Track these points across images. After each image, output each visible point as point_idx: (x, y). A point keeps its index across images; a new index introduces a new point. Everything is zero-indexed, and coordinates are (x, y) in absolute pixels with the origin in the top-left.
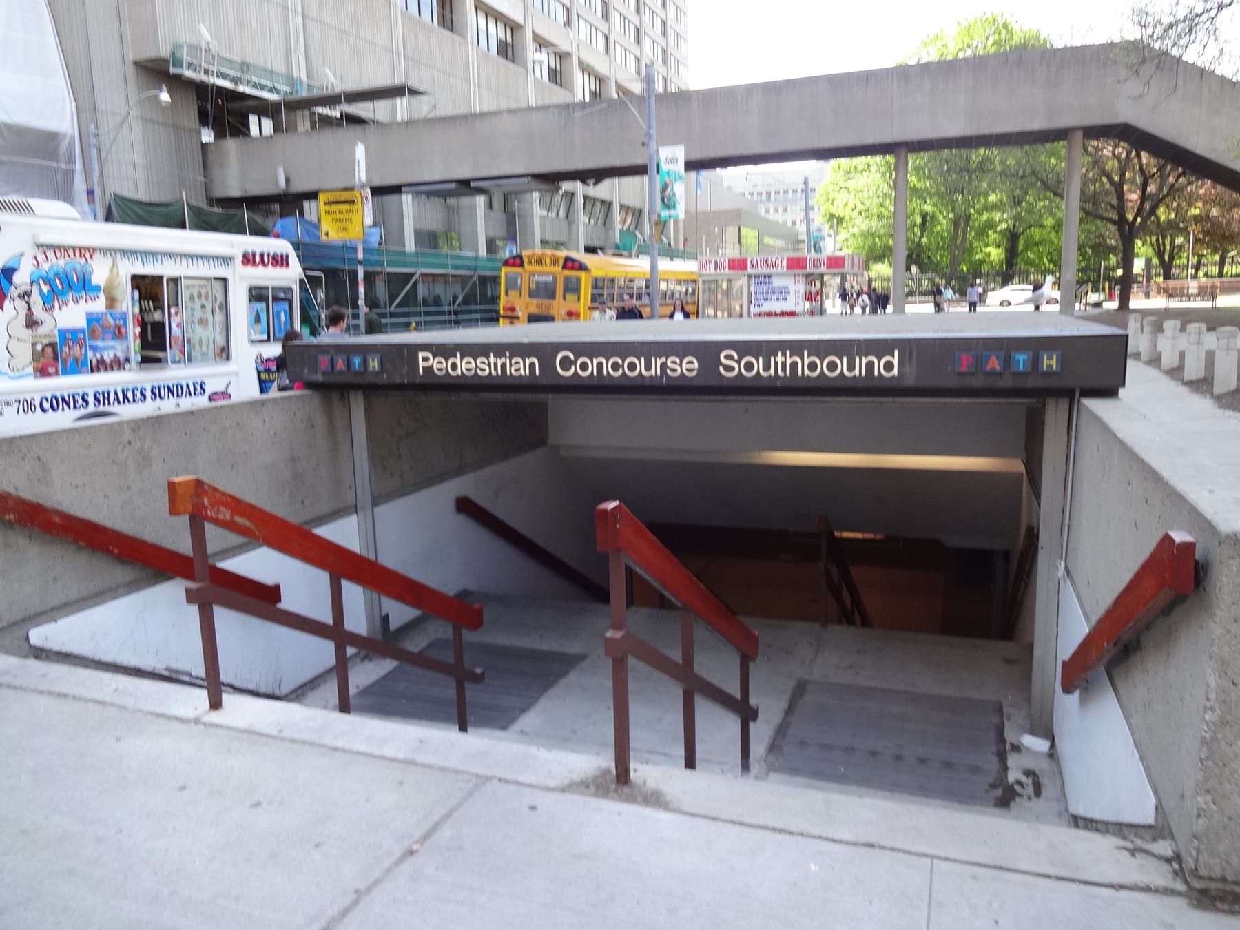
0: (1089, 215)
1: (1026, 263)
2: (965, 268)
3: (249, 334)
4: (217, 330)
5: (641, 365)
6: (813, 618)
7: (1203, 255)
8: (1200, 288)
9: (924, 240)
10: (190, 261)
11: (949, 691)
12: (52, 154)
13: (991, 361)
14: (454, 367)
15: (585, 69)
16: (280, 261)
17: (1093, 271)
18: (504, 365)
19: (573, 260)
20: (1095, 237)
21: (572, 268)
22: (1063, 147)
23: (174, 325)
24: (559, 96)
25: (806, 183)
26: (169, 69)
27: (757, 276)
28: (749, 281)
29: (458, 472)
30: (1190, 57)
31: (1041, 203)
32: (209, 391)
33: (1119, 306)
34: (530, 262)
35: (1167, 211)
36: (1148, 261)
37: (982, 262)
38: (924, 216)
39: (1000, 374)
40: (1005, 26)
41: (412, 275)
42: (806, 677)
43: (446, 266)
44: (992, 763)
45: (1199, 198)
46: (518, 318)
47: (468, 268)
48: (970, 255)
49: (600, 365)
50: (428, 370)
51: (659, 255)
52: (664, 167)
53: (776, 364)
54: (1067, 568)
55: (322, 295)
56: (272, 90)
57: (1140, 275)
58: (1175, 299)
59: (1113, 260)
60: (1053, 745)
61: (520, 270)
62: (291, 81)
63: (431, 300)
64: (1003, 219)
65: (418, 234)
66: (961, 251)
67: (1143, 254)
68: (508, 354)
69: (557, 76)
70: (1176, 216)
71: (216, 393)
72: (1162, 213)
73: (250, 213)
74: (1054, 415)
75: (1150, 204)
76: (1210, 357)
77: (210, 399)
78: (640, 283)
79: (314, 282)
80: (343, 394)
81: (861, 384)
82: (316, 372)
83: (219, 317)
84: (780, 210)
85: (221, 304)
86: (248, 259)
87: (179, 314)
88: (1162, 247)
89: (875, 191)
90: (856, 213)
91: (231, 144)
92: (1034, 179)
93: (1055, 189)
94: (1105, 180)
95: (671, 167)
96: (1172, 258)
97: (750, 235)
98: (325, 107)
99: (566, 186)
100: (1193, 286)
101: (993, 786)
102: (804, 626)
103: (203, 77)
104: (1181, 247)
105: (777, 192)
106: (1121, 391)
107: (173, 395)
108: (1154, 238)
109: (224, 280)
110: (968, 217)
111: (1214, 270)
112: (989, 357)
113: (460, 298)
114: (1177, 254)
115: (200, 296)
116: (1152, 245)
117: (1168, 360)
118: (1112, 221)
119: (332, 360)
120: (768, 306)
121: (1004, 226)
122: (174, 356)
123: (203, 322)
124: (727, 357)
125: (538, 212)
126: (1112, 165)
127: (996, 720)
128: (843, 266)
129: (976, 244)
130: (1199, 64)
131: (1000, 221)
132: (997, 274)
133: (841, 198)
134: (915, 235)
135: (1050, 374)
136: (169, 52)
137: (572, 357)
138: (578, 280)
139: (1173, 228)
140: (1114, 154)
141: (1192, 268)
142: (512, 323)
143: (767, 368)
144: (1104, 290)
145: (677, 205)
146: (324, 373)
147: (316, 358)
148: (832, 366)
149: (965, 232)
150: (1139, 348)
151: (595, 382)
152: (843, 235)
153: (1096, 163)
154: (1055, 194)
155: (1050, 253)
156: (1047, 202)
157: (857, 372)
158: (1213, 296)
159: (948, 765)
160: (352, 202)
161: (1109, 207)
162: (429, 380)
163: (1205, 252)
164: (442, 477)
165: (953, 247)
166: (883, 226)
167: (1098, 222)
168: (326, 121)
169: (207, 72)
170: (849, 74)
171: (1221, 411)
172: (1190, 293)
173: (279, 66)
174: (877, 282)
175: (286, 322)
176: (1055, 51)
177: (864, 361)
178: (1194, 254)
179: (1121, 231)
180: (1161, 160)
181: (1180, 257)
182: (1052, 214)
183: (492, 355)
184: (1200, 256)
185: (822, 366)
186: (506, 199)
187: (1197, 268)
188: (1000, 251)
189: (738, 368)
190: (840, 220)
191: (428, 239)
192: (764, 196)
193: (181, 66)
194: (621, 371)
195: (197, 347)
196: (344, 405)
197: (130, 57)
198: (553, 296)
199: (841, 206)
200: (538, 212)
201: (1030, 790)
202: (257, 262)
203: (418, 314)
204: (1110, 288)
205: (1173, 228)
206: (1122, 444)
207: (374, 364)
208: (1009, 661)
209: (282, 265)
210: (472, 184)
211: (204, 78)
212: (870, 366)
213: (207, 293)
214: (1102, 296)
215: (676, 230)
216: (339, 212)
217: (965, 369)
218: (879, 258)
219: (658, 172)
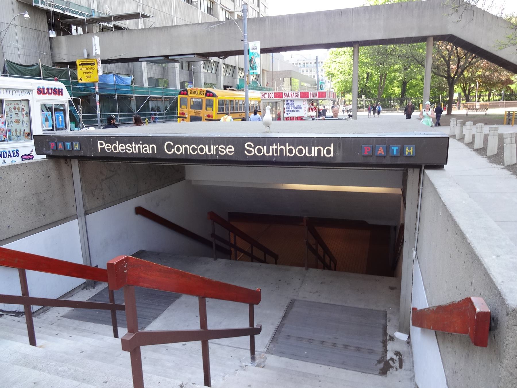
0: (436, 74)
1: (410, 94)
2: (384, 96)
3: (43, 127)
5: (206, 149)
8: (481, 106)
9: (368, 84)
11: (362, 306)
14: (115, 148)
18: (139, 147)
19: (210, 92)
20: (438, 84)
21: (209, 96)
24: (212, 19)
25: (317, 59)
27: (287, 101)
28: (283, 102)
29: (136, 195)
33: (447, 114)
35: (468, 73)
36: (460, 94)
37: (392, 94)
38: (368, 74)
39: (385, 157)
41: (147, 97)
42: (295, 298)
43: (161, 94)
44: (379, 348)
46: (186, 118)
48: (386, 91)
49: (186, 148)
50: (103, 149)
52: (251, 51)
53: (273, 149)
56: (81, 14)
57: (456, 100)
58: (470, 110)
59: (445, 93)
60: (409, 337)
61: (186, 96)
62: (90, 10)
64: (400, 76)
65: (149, 79)
66: (383, 89)
68: (141, 142)
71: (25, 155)
72: (466, 74)
75: (461, 69)
76: (486, 137)
77: (23, 159)
79: (76, 102)
80: (66, 160)
81: (314, 161)
82: (49, 150)
86: (40, 91)
89: (347, 63)
92: (412, 59)
93: (421, 63)
94: (442, 59)
96: (469, 93)
97: (295, 81)
98: (106, 23)
99: (213, 59)
100: (478, 105)
101: (379, 362)
102: (297, 269)
104: (473, 88)
105: (307, 63)
106: (445, 166)
108: (462, 84)
109: (27, 101)
110: (386, 74)
111: (486, 98)
114: (471, 91)
115: (15, 109)
116: (461, 87)
117: (468, 139)
119: (56, 143)
120: (292, 114)
121: (401, 78)
123: (17, 121)
124: (248, 146)
125: (203, 70)
126: (445, 53)
127: (383, 322)
128: (325, 97)
129: (389, 86)
131: (399, 76)
132: (397, 99)
133: (333, 65)
134: (364, 82)
135: (409, 157)
137: (172, 144)
138: (212, 101)
139: (471, 80)
141: (477, 97)
142: (183, 120)
143: (268, 152)
146: (53, 150)
147: (49, 143)
148: (300, 151)
149: (384, 81)
150: (455, 133)
151: (184, 158)
152: (334, 81)
153: (439, 51)
155: (419, 90)
157: (313, 155)
158: (486, 109)
159: (358, 349)
160: (92, 64)
161: (444, 71)
164: (127, 198)
165: (380, 87)
166: (350, 78)
168: (105, 29)
169: (50, 5)
170: (334, 11)
171: (491, 164)
172: (476, 108)
174: (348, 102)
175: (62, 121)
177: (316, 148)
178: (478, 91)
179: (448, 81)
180: (466, 51)
182: (420, 74)
184: (481, 92)
185: (295, 151)
187: (479, 97)
188: (399, 89)
189: (254, 151)
190: (332, 75)
191: (154, 82)
192: (302, 65)
194: (196, 152)
195: (14, 133)
196: (68, 166)
198: (201, 109)
199: (333, 69)
200: (203, 70)
201: (397, 364)
202: (45, 92)
203: (149, 115)
205: (471, 80)
206: (444, 205)
207: (76, 146)
209: (59, 94)
210: (170, 58)
211: (49, 8)
212: (319, 151)
215: (263, 79)
216: (87, 69)
218: (349, 92)
219: (248, 54)
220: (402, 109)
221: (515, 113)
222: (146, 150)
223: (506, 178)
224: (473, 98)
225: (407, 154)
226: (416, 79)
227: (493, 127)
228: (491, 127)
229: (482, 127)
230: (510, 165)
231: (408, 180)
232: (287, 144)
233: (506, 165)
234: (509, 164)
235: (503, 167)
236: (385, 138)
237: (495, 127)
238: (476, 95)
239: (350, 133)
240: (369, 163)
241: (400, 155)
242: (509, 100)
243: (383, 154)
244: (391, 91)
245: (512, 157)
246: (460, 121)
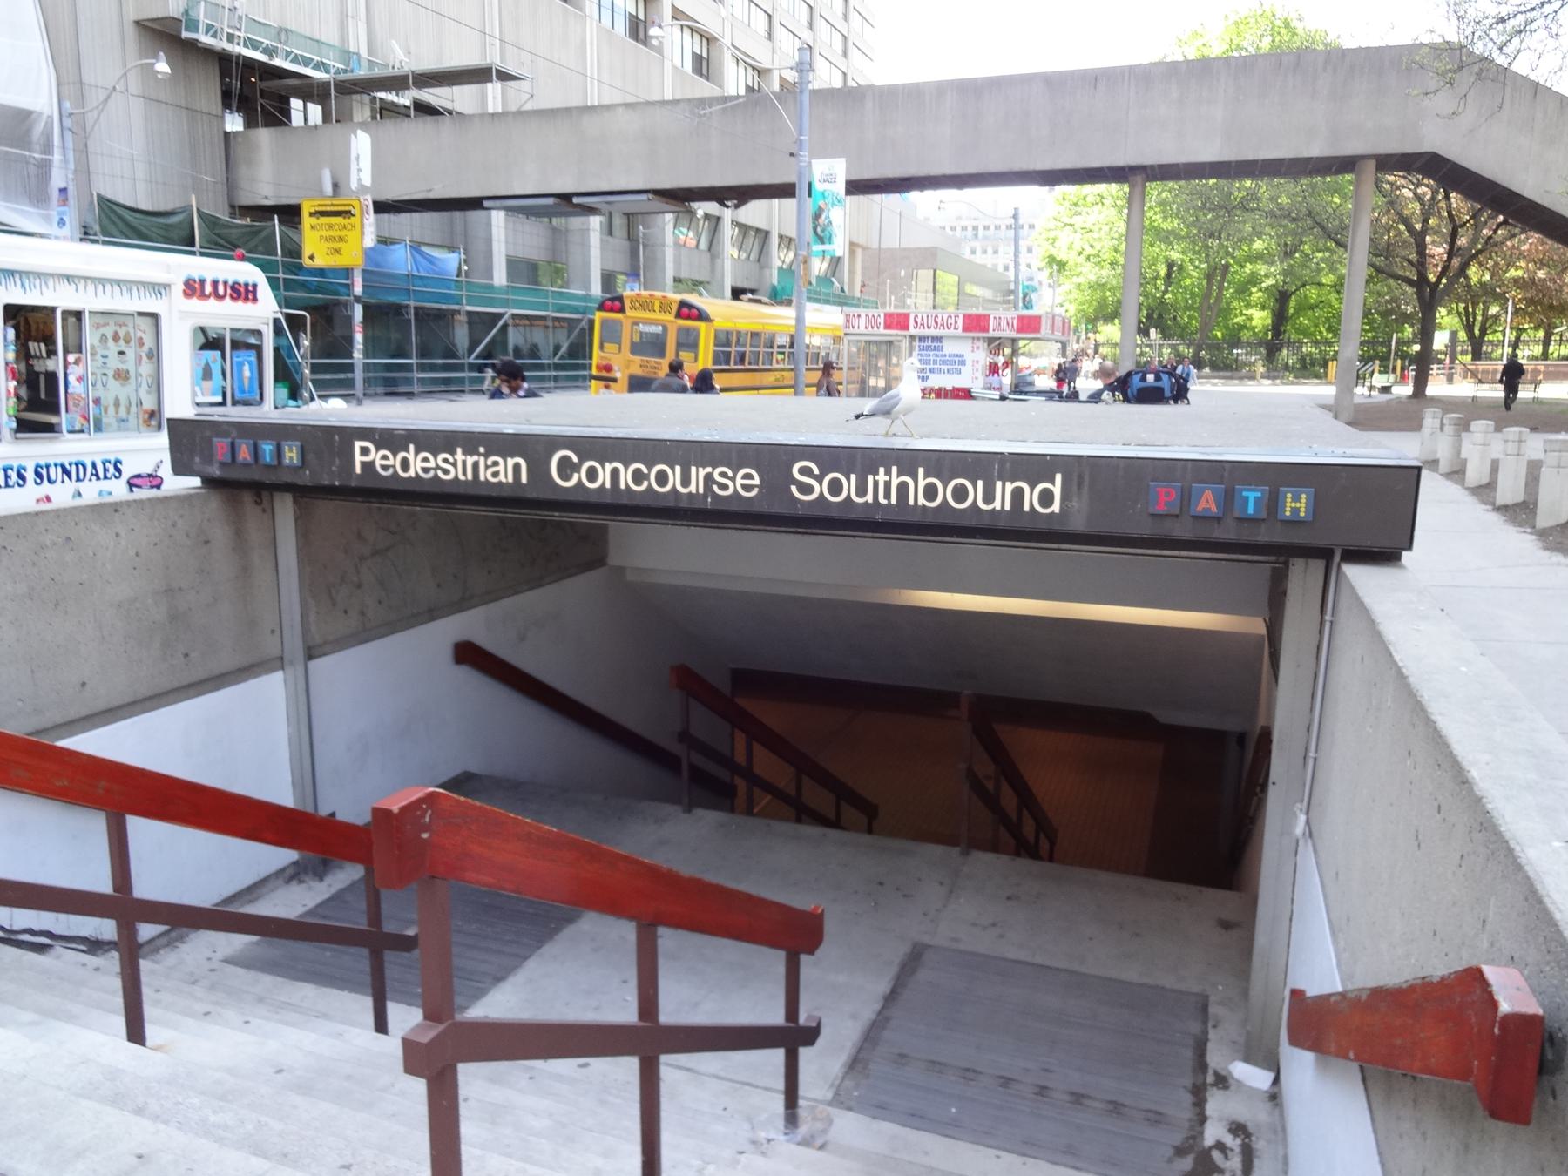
0: (1380, 272)
1: (1298, 331)
3: (194, 394)
4: (144, 387)
5: (675, 477)
6: (949, 840)
7: (1525, 330)
10: (100, 287)
11: (1131, 973)
12: (23, 141)
13: (1204, 499)
14: (405, 464)
15: (743, 59)
16: (243, 292)
17: (1382, 344)
18: (476, 466)
19: (690, 306)
21: (688, 317)
22: (1350, 182)
23: (72, 378)
24: (704, 89)
26: (180, 33)
27: (922, 339)
28: (910, 343)
30: (1520, 67)
31: (1320, 255)
32: (128, 472)
34: (633, 308)
36: (1454, 334)
37: (1242, 327)
38: (1170, 265)
39: (1218, 519)
40: (1287, 25)
41: (500, 316)
42: (926, 939)
43: (545, 306)
44: (1179, 1106)
45: (1521, 256)
46: (615, 380)
47: (575, 310)
48: (1226, 319)
49: (615, 472)
50: (368, 467)
51: (809, 299)
53: (876, 484)
54: (1308, 822)
55: (306, 342)
59: (1409, 331)
60: (1276, 1081)
62: (346, 55)
63: (525, 350)
64: (1271, 275)
65: (512, 264)
67: (1447, 326)
68: (482, 450)
69: (702, 66)
70: (1491, 278)
72: (1473, 271)
73: (283, 228)
74: (1303, 579)
75: (1459, 259)
78: (782, 340)
79: (295, 323)
81: (1002, 524)
83: (146, 368)
84: (990, 251)
85: (150, 349)
86: (193, 288)
87: (81, 365)
90: (1083, 257)
91: (264, 135)
93: (1337, 237)
94: (1402, 227)
95: (826, 186)
96: (1483, 332)
97: (948, 281)
99: (702, 208)
101: (1180, 1152)
102: (936, 850)
103: (222, 44)
104: (1496, 318)
105: (986, 228)
106: (1406, 556)
107: (70, 477)
108: (1462, 305)
109: (154, 316)
112: (1202, 492)
113: (564, 349)
115: (116, 338)
116: (1459, 313)
118: (1410, 282)
119: (233, 446)
121: (1270, 282)
122: (71, 423)
123: (122, 376)
124: (803, 471)
126: (1414, 208)
127: (1195, 1027)
130: (1532, 77)
131: (1266, 276)
132: (1260, 344)
133: (1065, 237)
134: (1157, 289)
135: (1294, 523)
136: (182, 10)
137: (575, 459)
138: (697, 332)
139: (1489, 293)
140: (1415, 194)
142: (607, 387)
143: (862, 491)
144: (1394, 370)
145: (834, 238)
146: (223, 465)
147: (210, 442)
149: (1221, 288)
150: (1436, 452)
151: (608, 500)
153: (1391, 203)
154: (1339, 244)
156: (1327, 254)
159: (1116, 1108)
162: (369, 484)
163: (1526, 326)
164: (432, 614)
167: (1392, 282)
169: (230, 38)
170: (1073, 72)
171: (1547, 554)
173: (330, 35)
175: (251, 379)
176: (1344, 53)
177: (1009, 487)
179: (1420, 294)
182: (1332, 270)
183: (459, 450)
184: (1521, 331)
185: (945, 493)
186: (630, 217)
188: (1265, 313)
189: (821, 489)
190: (1062, 265)
191: (524, 270)
192: (970, 233)
193: (196, 30)
194: (576, 477)
196: (264, 511)
197: (132, 15)
204: (1403, 369)
205: (1489, 293)
206: (1401, 676)
207: (291, 455)
208: (1226, 925)
209: (246, 299)
210: (575, 200)
212: (1018, 495)
213: (127, 334)
214: (1392, 377)
216: (330, 227)
217: (1164, 510)
218: (1110, 317)
220: (1272, 374)
222: (495, 474)
225: (1288, 514)
226: (1320, 284)
227: (1557, 441)
232: (921, 471)
241: (1177, 512)
243: (1214, 510)
244: (1239, 320)
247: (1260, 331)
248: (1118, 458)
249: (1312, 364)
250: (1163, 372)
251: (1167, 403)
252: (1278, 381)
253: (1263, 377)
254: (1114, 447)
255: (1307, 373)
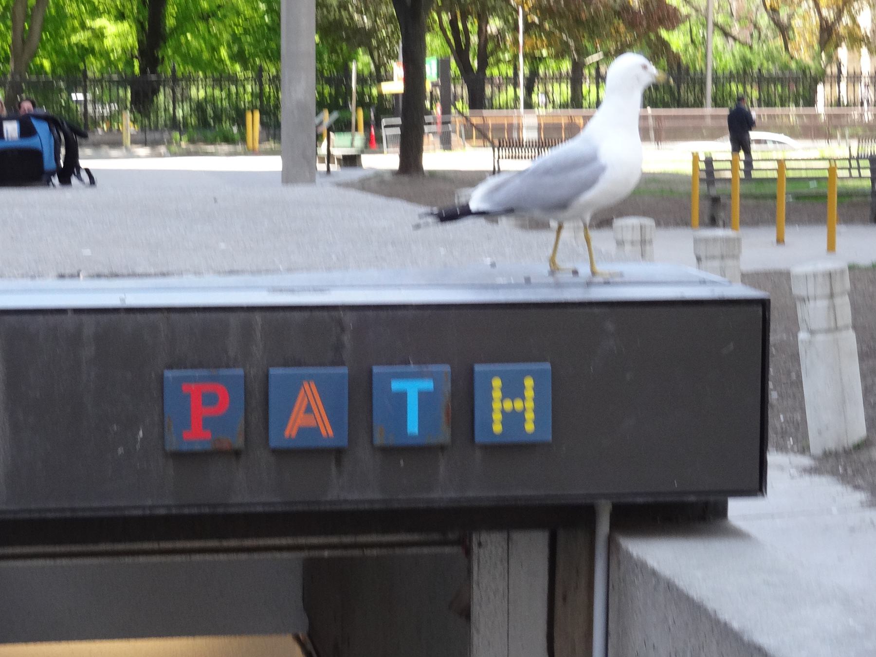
2: (47, 64)
7: (541, 59)
37: (85, 51)
39: (338, 454)
48: (56, 35)
88: (463, 38)
108: (446, 18)
111: (562, 91)
163: (545, 52)
181: (499, 61)
220: (150, 136)
221: (791, 180)
223: (852, 530)
224: (496, 90)
225: (497, 428)
227: (715, 240)
228: (706, 241)
229: (648, 238)
230: (841, 449)
231: (475, 610)
233: (816, 447)
234: (831, 445)
235: (805, 461)
236: (334, 313)
237: (727, 240)
238: (516, 74)
239: (33, 277)
240: (221, 510)
241: (239, 442)
242: (666, 105)
243: (327, 430)
244: (79, 38)
245: (844, 402)
246: (457, 211)
247: (119, 59)
248: (79, 311)
249: (218, 118)
250: (38, 117)
251: (48, 183)
252: (162, 149)
253: (135, 142)
254: (39, 283)
255: (209, 134)
